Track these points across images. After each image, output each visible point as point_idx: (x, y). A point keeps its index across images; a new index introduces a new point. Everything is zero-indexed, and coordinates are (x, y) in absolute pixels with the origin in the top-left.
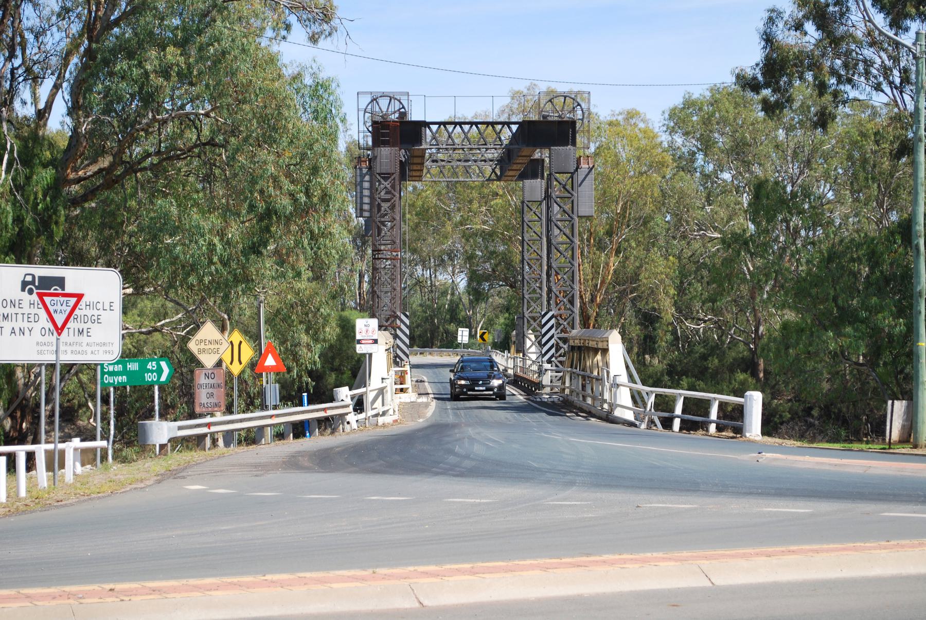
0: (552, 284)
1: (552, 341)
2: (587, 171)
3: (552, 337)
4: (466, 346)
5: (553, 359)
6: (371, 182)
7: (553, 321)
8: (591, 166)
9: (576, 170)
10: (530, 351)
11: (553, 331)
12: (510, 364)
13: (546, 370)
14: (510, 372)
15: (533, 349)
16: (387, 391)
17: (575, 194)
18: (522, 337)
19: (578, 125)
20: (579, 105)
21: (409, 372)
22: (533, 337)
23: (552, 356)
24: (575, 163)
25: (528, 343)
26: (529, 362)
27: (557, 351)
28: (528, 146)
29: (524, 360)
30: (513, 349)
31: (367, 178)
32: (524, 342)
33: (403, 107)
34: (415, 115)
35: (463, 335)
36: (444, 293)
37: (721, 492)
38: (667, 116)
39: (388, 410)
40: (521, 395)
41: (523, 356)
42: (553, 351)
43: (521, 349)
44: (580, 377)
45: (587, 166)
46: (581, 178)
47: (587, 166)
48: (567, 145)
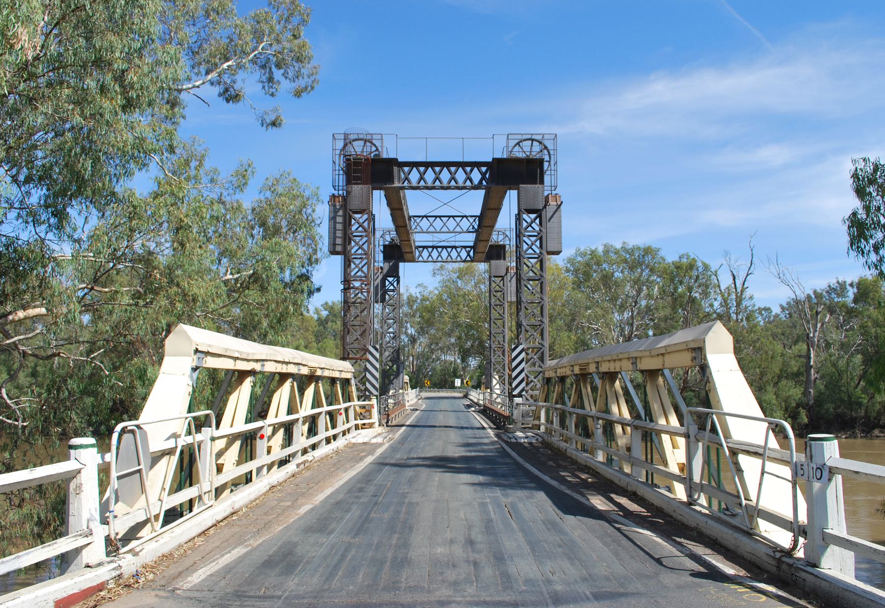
0: (522, 318)
1: (523, 375)
2: (555, 208)
3: (522, 371)
4: (459, 388)
5: (524, 393)
6: (344, 216)
7: (523, 355)
8: (559, 203)
9: (545, 207)
10: (496, 387)
11: (523, 365)
12: (481, 397)
13: (517, 404)
14: (481, 402)
15: (498, 386)
16: (79, 487)
17: (544, 230)
18: (490, 378)
19: (546, 165)
20: (546, 148)
21: (375, 406)
22: (497, 377)
23: (523, 390)
24: (544, 200)
25: (494, 382)
26: (495, 396)
27: (527, 384)
28: (497, 184)
29: (491, 394)
30: (483, 387)
31: (341, 213)
32: (491, 381)
33: (377, 150)
34: (388, 153)
35: (458, 382)
36: (451, 363)
37: (598, 473)
38: (566, 262)
39: (78, 551)
40: (491, 428)
41: (491, 390)
42: (524, 384)
43: (489, 386)
44: (839, 478)
45: (555, 204)
46: (549, 215)
47: (555, 204)
48: (536, 184)
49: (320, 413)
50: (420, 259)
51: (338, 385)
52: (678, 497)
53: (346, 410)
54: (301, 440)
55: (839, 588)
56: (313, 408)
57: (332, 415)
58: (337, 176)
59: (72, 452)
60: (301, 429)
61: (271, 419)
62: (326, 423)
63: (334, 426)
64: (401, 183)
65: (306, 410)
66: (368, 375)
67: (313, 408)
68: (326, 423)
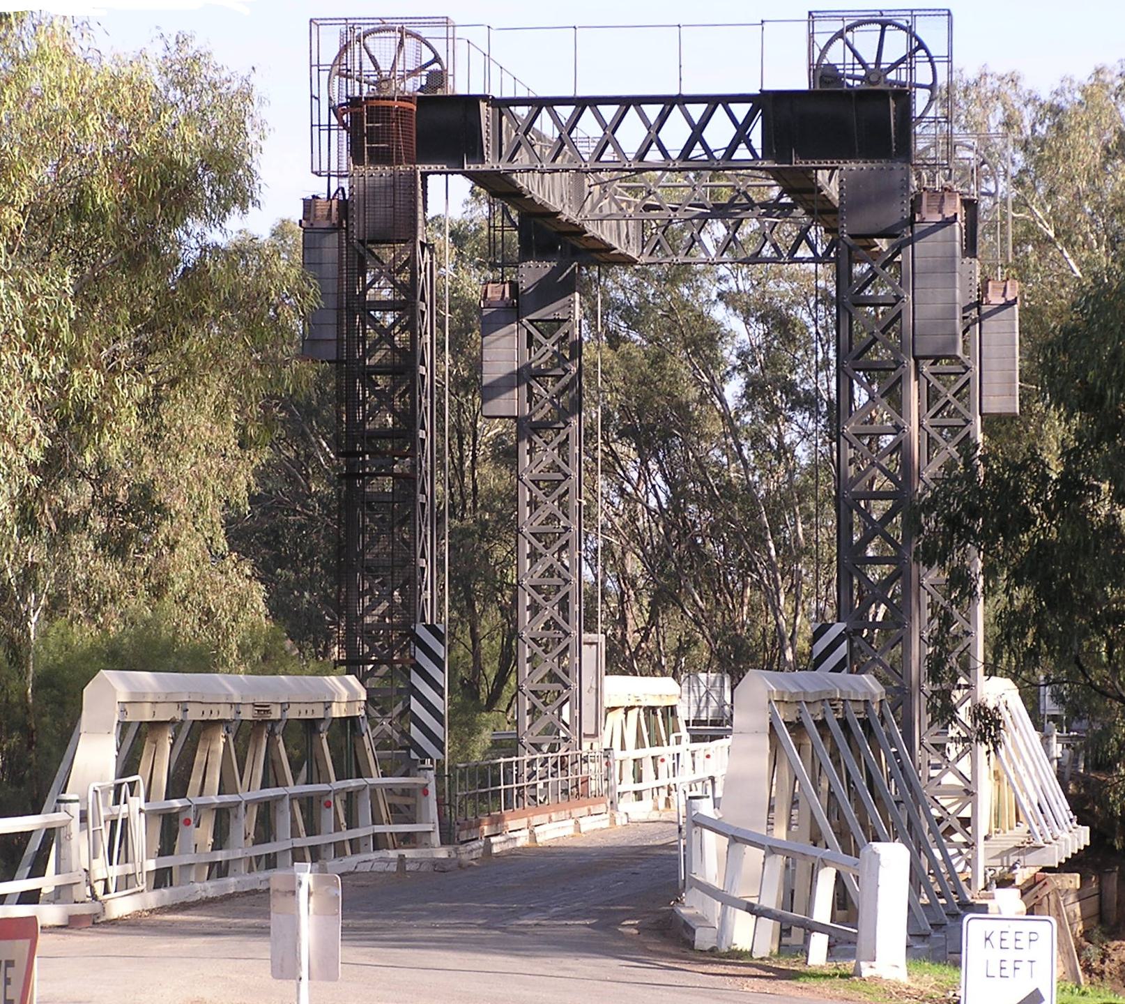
33: (437, 59)
49: (279, 799)
50: (741, 110)
51: (324, 735)
52: (708, 881)
53: (351, 798)
54: (240, 848)
55: (566, 854)
56: (264, 785)
57: (309, 805)
58: (324, 134)
59: (62, 805)
60: (245, 823)
61: (193, 798)
62: (294, 821)
63: (312, 830)
64: (505, 158)
65: (252, 791)
66: (415, 706)
67: (264, 785)
68: (294, 821)
